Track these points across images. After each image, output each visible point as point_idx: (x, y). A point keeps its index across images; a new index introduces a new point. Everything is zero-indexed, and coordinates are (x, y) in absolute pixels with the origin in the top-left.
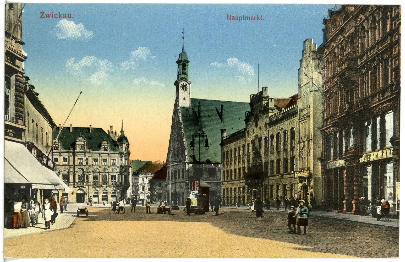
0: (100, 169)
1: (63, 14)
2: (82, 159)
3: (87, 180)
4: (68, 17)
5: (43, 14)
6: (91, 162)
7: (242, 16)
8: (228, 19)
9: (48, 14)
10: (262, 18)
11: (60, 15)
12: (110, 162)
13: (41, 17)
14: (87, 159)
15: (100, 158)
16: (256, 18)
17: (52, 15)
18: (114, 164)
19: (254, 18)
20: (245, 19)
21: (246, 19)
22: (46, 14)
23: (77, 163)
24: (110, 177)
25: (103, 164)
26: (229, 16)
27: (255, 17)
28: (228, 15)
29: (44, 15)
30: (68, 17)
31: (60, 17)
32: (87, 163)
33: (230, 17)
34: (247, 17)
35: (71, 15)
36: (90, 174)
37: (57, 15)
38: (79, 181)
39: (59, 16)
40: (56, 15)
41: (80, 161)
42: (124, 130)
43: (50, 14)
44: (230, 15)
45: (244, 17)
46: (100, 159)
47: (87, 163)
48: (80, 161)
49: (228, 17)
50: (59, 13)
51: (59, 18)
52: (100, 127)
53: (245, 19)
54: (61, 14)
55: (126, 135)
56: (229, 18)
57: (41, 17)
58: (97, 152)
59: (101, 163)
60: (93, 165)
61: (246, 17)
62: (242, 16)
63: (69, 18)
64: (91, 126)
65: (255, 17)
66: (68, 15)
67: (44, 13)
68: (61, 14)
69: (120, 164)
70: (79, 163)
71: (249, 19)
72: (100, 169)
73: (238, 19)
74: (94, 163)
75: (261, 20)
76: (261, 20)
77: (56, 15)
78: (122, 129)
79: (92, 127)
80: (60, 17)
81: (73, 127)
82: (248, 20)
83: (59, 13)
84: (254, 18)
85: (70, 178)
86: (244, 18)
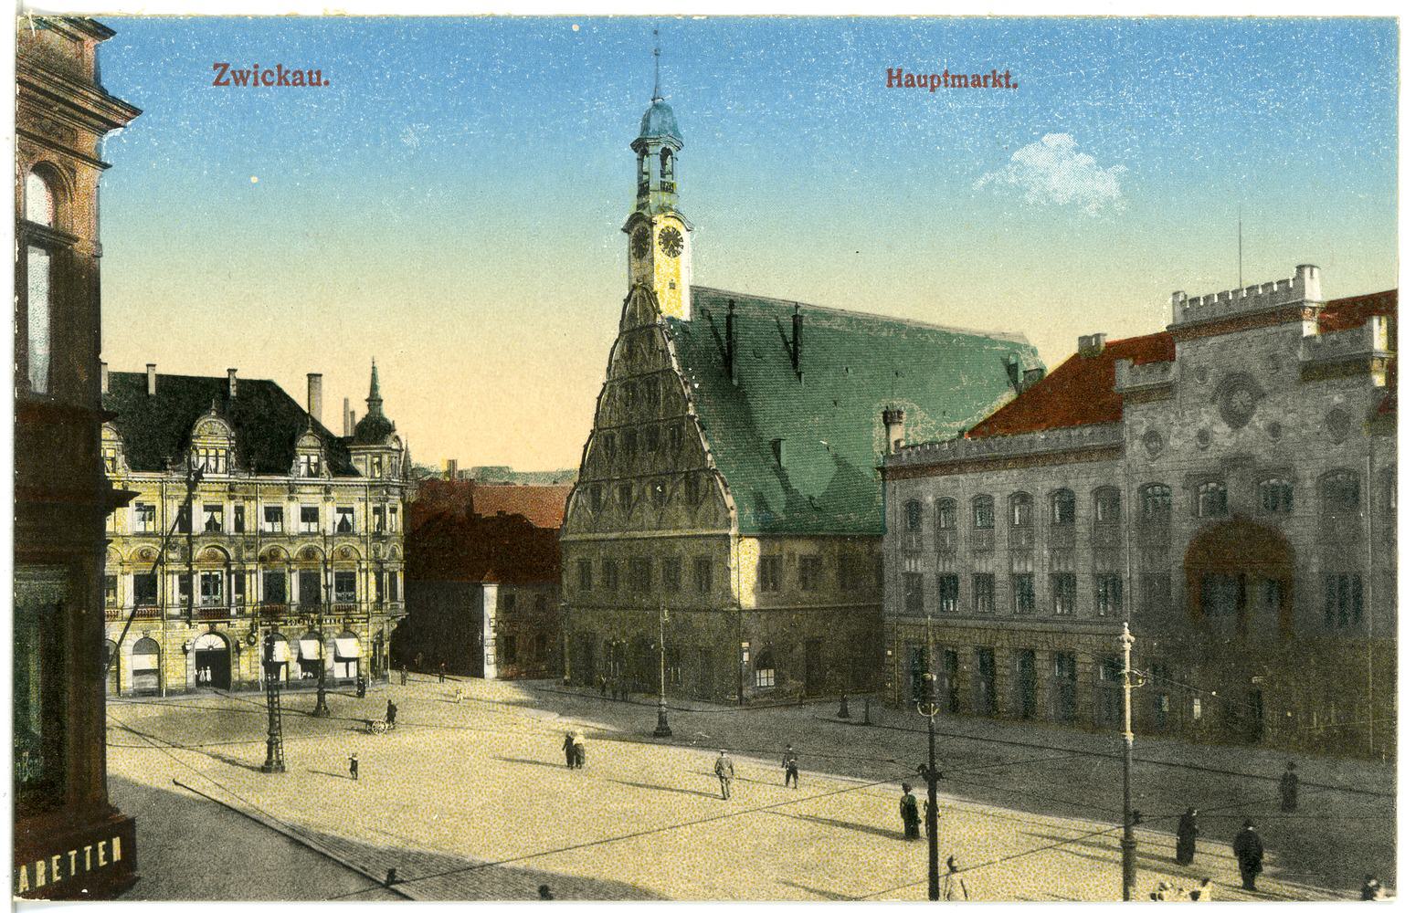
0: (290, 549)
1: (292, 72)
2: (220, 509)
3: (239, 596)
4: (311, 79)
5: (223, 71)
6: (255, 518)
7: (940, 73)
8: (890, 85)
9: (241, 72)
10: (1011, 81)
11: (283, 73)
12: (329, 518)
13: (217, 83)
14: (240, 510)
15: (329, 504)
16: (991, 81)
17: (256, 73)
18: (345, 528)
19: (982, 80)
20: (950, 81)
21: (960, 85)
22: (233, 73)
23: (199, 520)
24: (331, 578)
25: (303, 527)
26: (895, 73)
27: (986, 78)
28: (890, 71)
29: (228, 75)
30: (311, 79)
31: (283, 82)
32: (239, 526)
33: (899, 76)
34: (959, 77)
35: (318, 73)
36: (251, 572)
37: (272, 74)
38: (204, 602)
39: (280, 78)
40: (268, 75)
41: (212, 517)
42: (382, 393)
43: (249, 72)
44: (900, 71)
45: (946, 74)
46: (292, 511)
47: (239, 526)
48: (212, 517)
49: (890, 78)
50: (279, 67)
51: (280, 84)
52: (265, 377)
53: (950, 81)
54: (287, 72)
55: (389, 412)
56: (895, 82)
57: (217, 83)
58: (282, 479)
59: (294, 523)
60: (263, 534)
61: (953, 77)
62: (940, 73)
63: (312, 84)
64: (231, 371)
65: (986, 78)
66: (310, 73)
67: (226, 66)
68: (287, 72)
69: (372, 529)
70: (208, 525)
71: (966, 86)
72: (290, 549)
73: (925, 85)
74: (268, 527)
75: (1008, 86)
76: (1008, 86)
77: (268, 75)
78: (374, 387)
79: (241, 375)
80: (283, 82)
81: (159, 377)
82: (960, 85)
83: (279, 67)
84: (982, 80)
85: (170, 590)
86: (946, 81)
